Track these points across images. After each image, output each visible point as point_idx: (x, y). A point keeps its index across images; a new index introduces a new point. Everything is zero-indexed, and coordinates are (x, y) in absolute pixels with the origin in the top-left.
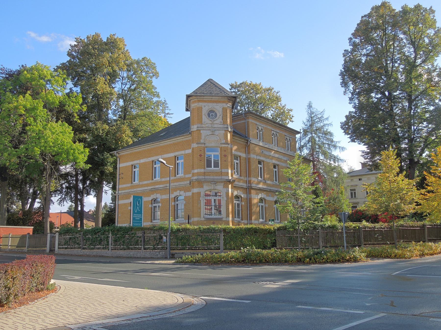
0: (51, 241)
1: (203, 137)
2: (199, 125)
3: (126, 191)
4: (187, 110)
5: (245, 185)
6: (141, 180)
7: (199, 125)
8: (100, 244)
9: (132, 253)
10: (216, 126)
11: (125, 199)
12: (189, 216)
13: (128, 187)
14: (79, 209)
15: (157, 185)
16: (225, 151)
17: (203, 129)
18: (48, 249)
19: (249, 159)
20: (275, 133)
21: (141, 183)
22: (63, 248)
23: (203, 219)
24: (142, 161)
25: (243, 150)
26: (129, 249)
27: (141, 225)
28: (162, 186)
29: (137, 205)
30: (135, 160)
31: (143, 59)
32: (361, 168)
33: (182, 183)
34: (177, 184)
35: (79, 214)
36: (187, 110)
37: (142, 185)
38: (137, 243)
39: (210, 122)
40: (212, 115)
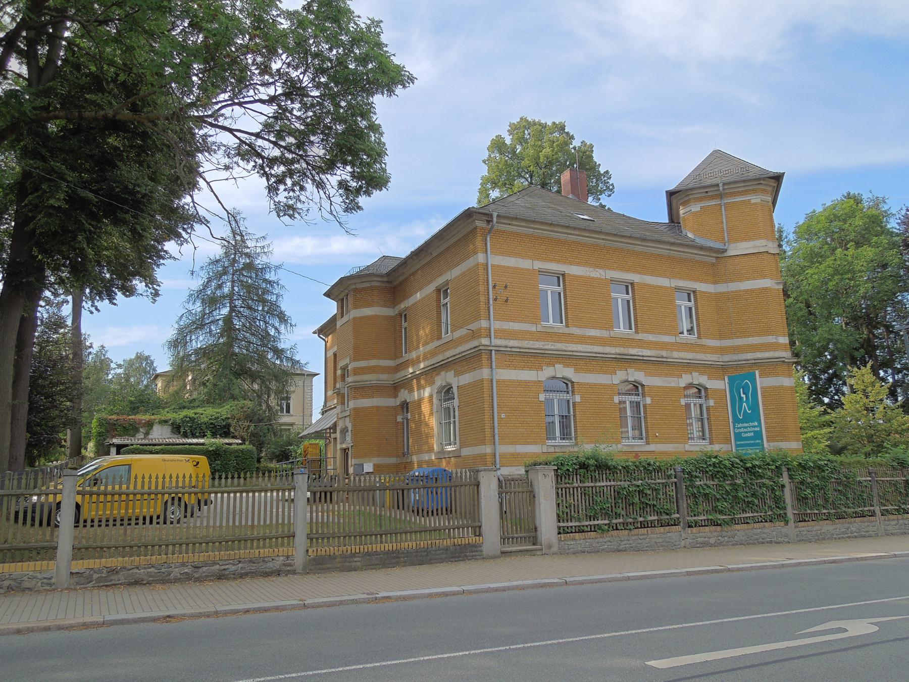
15: (633, 347)
22: (581, 531)
29: (741, 398)
30: (551, 261)
38: (861, 500)
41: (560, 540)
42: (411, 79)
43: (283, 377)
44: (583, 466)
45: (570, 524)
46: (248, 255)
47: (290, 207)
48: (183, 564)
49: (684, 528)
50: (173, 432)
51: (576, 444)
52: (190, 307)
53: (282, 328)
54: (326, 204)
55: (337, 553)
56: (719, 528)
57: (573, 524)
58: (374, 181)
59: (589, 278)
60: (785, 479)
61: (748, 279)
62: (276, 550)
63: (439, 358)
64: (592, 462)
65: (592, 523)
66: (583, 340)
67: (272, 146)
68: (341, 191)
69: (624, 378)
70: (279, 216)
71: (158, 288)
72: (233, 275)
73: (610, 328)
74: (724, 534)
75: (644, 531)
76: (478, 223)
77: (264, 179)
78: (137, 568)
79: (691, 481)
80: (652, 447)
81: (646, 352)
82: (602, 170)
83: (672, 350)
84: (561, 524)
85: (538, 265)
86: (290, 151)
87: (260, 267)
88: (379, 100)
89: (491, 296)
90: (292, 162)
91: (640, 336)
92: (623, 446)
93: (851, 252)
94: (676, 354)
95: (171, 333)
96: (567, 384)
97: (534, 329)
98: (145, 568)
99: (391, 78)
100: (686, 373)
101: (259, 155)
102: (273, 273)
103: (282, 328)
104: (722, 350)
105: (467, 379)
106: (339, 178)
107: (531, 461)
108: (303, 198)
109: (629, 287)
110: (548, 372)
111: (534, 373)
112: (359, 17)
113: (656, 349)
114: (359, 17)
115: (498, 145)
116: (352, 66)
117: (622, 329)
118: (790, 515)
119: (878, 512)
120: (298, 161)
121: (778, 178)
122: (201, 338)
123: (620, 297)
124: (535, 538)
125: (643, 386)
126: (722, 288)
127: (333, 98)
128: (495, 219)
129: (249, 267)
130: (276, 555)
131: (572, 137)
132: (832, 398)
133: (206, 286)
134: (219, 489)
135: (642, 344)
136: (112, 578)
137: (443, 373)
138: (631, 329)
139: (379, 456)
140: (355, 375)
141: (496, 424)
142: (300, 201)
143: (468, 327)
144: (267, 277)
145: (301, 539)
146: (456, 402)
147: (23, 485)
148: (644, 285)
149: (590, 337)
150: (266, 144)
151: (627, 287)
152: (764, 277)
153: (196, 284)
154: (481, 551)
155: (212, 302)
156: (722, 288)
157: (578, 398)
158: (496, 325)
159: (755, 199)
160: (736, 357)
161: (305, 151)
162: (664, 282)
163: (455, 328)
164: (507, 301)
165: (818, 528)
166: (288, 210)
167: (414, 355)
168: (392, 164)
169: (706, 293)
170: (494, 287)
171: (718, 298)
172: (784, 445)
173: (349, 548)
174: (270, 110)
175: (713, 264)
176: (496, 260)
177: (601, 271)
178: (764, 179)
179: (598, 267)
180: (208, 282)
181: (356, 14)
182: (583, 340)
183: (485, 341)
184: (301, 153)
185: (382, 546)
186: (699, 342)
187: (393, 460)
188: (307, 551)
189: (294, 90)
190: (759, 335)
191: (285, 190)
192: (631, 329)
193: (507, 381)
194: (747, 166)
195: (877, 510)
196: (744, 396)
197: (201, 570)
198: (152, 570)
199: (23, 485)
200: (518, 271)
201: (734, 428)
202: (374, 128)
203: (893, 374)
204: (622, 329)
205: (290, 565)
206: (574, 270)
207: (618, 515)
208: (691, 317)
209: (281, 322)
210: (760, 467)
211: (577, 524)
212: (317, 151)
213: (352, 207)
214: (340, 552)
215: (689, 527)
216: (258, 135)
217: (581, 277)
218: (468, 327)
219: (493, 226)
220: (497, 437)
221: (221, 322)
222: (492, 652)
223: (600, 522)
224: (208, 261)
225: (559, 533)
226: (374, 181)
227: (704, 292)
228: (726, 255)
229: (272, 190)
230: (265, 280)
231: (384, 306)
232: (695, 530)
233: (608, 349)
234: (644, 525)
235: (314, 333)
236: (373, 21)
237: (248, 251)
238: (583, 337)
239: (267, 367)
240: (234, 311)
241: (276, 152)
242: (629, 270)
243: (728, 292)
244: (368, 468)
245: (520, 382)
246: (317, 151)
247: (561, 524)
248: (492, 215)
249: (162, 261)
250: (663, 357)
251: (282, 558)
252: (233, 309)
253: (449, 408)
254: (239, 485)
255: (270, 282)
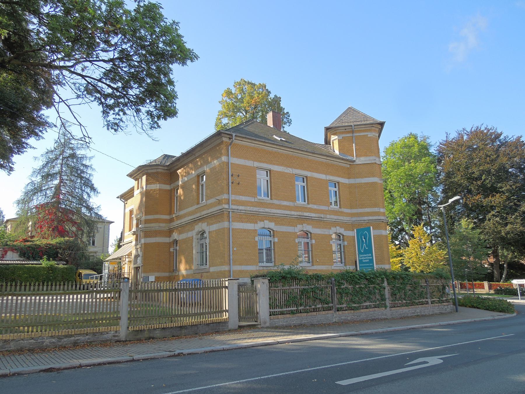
3: (248, 208)
8: (368, 299)
9: (419, 309)
11: (246, 222)
15: (306, 212)
22: (282, 313)
26: (413, 304)
28: (317, 215)
29: (363, 241)
30: (263, 162)
33: (341, 218)
34: (336, 217)
38: (421, 295)
41: (271, 319)
42: (197, 57)
43: (95, 225)
44: (284, 278)
45: (276, 310)
46: (72, 149)
47: (116, 124)
48: (52, 337)
49: (335, 312)
50: (20, 256)
51: (275, 266)
52: (34, 179)
53: (92, 194)
54: (140, 124)
55: (145, 329)
56: (352, 311)
57: (278, 310)
58: (168, 112)
59: (284, 172)
60: (385, 284)
61: (366, 177)
62: (109, 328)
63: (198, 215)
64: (289, 276)
65: (288, 309)
66: (279, 207)
67: (107, 87)
68: (148, 117)
69: (263, 226)
70: (108, 129)
71: (12, 166)
72: (63, 160)
73: (254, 195)
74: (355, 314)
75: (314, 313)
76: (224, 139)
77: (101, 106)
78: (23, 340)
79: (339, 286)
80: (315, 267)
81: (313, 215)
82: (285, 111)
83: (326, 214)
84: (272, 310)
85: (256, 164)
86: (118, 91)
87: (80, 156)
88: (175, 67)
89: (230, 181)
90: (119, 97)
91: (310, 206)
92: (304, 265)
93: (412, 164)
94: (328, 216)
95: (19, 195)
96: (270, 232)
97: (253, 200)
98: (27, 340)
99: (184, 55)
100: (333, 226)
101: (99, 92)
102: (88, 160)
103: (92, 194)
104: (352, 215)
105: (215, 227)
106: (148, 109)
107: (255, 274)
108: (124, 119)
109: (305, 179)
110: (260, 224)
111: (252, 225)
112: (166, 18)
113: (318, 213)
114: (166, 18)
115: (229, 93)
116: (161, 45)
117: (300, 202)
118: (388, 304)
119: (430, 302)
120: (123, 97)
121: (382, 124)
122: (40, 198)
123: (299, 184)
124: (257, 318)
125: (311, 233)
126: (352, 181)
127: (148, 62)
128: (234, 137)
129: (73, 156)
130: (110, 332)
131: (269, 92)
132: (400, 241)
133: (44, 167)
134: (30, 292)
135: (311, 210)
136: (6, 346)
137: (200, 224)
138: (305, 201)
139: (158, 272)
140: (145, 223)
141: (231, 254)
142: (122, 121)
143: (217, 198)
144: (84, 163)
145: (124, 321)
146: (207, 241)
147: (45, 289)
148: (312, 178)
149: (284, 206)
150: (104, 86)
151: (335, 184)
152: (374, 176)
153: (39, 164)
154: (228, 326)
155: (47, 177)
156: (352, 181)
157: (276, 240)
158: (233, 197)
159: (370, 135)
160: (358, 219)
161: (127, 92)
162: (323, 177)
163: (208, 198)
164: (238, 184)
165: (401, 310)
166: (115, 126)
167: (182, 213)
168: (179, 104)
169: (344, 183)
170: (232, 175)
171: (351, 186)
172: (383, 266)
173: (153, 326)
174: (108, 66)
175: (348, 168)
176: (234, 160)
177: (290, 169)
178: (375, 124)
179: (289, 167)
180: (46, 164)
181: (165, 17)
182: (279, 207)
183: (226, 206)
184: (124, 93)
185: (172, 324)
186: (340, 210)
187: (167, 274)
188: (128, 328)
189: (125, 56)
190: (371, 207)
191: (113, 114)
192: (305, 201)
193: (237, 229)
194: (365, 117)
195: (429, 301)
196: (364, 240)
197: (63, 340)
198: (32, 341)
199: (45, 289)
200: (244, 167)
201: (359, 257)
202: (171, 82)
203: (431, 229)
204: (300, 202)
205: (117, 336)
206: (275, 168)
207: (301, 305)
208: (336, 196)
209: (91, 189)
210: (373, 278)
211: (280, 310)
212: (134, 91)
213: (155, 125)
214: (148, 328)
215: (338, 311)
216: (100, 80)
217: (279, 172)
218: (217, 198)
219: (232, 142)
220: (231, 261)
221: (53, 189)
222: (252, 381)
223: (292, 309)
224: (46, 151)
225: (270, 315)
226: (168, 112)
227: (343, 183)
228: (355, 163)
229: (105, 113)
230: (83, 165)
231: (164, 184)
232: (340, 312)
233: (293, 213)
234: (315, 310)
235: (118, 198)
236: (174, 22)
237: (73, 146)
238: (280, 205)
239: (81, 217)
240: (62, 182)
241: (110, 91)
242: (339, 176)
243: (355, 184)
244: (152, 278)
245: (245, 230)
246: (134, 91)
247: (272, 310)
248: (232, 135)
249: (25, 150)
250: (321, 218)
251: (112, 332)
252: (61, 181)
253: (203, 244)
254: (55, 290)
255: (86, 166)
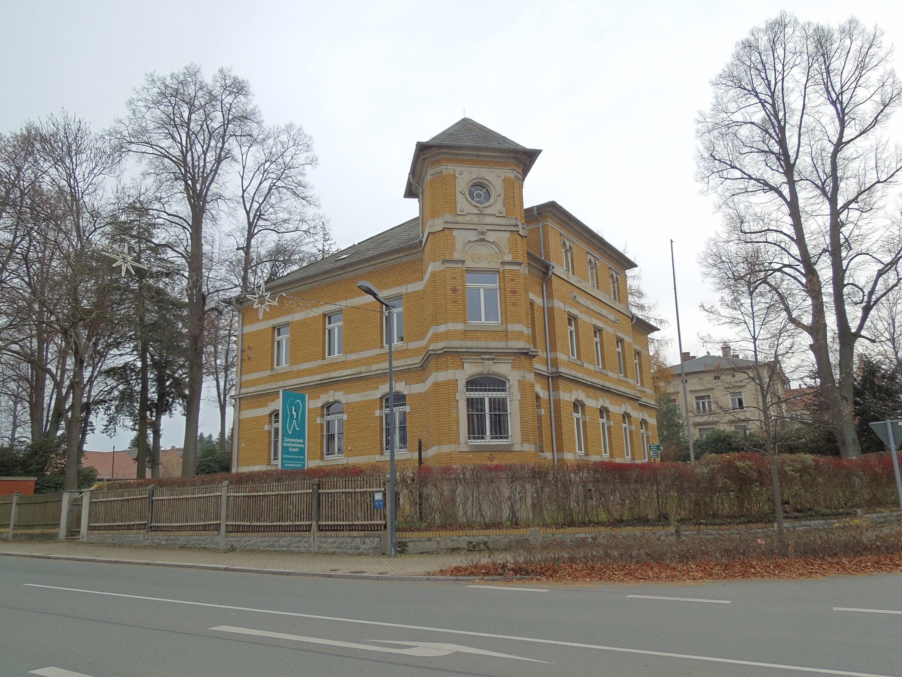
0: (70, 512)
1: (459, 246)
2: (449, 218)
4: (410, 193)
5: (544, 368)
6: (294, 359)
7: (449, 218)
10: (489, 220)
12: (420, 442)
13: (263, 378)
14: (151, 439)
16: (513, 280)
17: (458, 226)
18: (62, 531)
19: (551, 310)
20: (592, 259)
21: (295, 368)
23: (465, 449)
24: (298, 316)
25: (538, 288)
27: (303, 465)
29: (292, 415)
31: (290, 127)
32: (680, 363)
35: (146, 452)
36: (410, 193)
37: (298, 371)
39: (476, 211)
40: (479, 196)
